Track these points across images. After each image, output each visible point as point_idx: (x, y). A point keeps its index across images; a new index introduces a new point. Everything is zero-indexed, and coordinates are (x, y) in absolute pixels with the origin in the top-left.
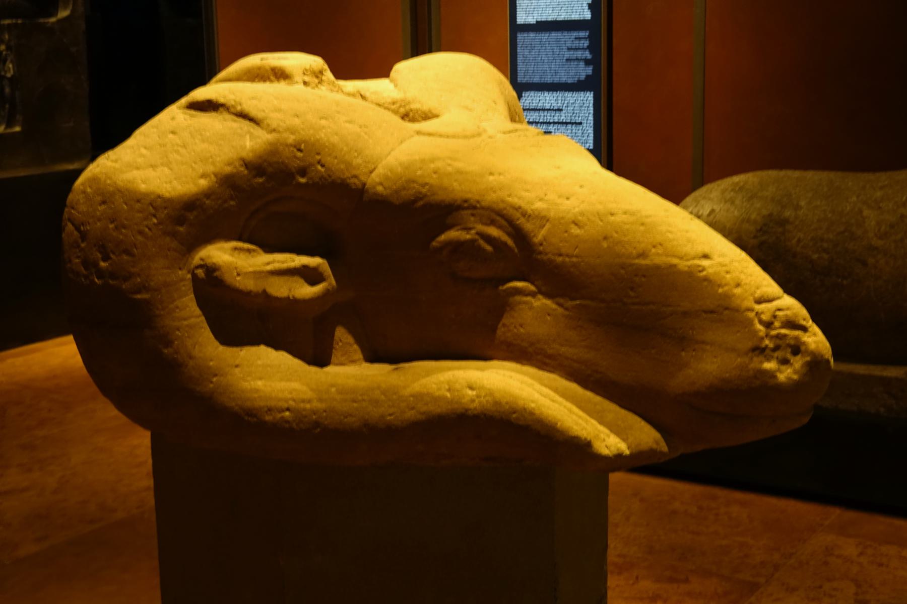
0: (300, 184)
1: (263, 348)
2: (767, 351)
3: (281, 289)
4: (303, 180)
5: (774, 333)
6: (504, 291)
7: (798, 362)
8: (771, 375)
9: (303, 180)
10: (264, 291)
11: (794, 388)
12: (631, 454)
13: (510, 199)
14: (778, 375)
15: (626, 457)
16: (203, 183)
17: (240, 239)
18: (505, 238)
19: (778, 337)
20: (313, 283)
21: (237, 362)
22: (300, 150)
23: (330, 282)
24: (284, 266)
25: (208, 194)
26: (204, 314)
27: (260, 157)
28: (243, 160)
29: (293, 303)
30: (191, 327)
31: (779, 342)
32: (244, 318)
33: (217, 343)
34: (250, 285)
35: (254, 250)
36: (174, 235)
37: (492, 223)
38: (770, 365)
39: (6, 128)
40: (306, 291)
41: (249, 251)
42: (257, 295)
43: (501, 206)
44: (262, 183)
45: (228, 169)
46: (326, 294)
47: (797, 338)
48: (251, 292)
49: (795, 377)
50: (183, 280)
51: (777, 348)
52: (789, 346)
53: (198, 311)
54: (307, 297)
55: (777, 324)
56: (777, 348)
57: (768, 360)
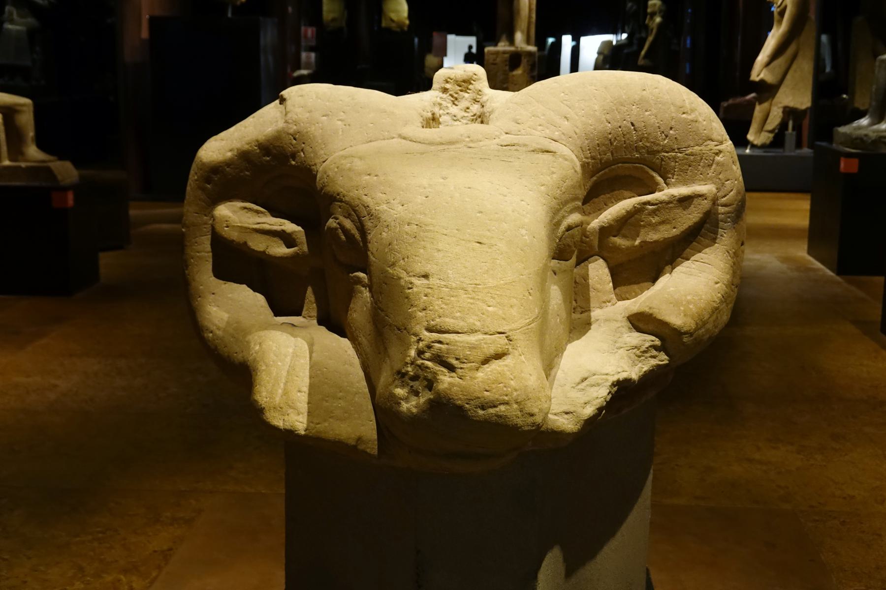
0: (292, 165)
1: (244, 286)
2: (406, 378)
3: (258, 244)
4: (293, 163)
5: (420, 362)
6: (352, 278)
7: (426, 396)
8: (397, 400)
9: (293, 163)
10: (245, 243)
11: (413, 420)
12: (305, 436)
13: (365, 198)
14: (403, 403)
15: (299, 436)
16: (229, 154)
17: (244, 200)
18: (355, 232)
19: (422, 367)
20: (289, 246)
21: (214, 292)
22: (295, 139)
23: (304, 247)
24: (267, 227)
25: (228, 163)
26: (213, 251)
27: (268, 141)
28: (257, 141)
29: (282, 259)
30: (200, 258)
31: (420, 372)
32: (237, 262)
33: (211, 274)
34: (234, 236)
35: (262, 213)
36: (203, 189)
37: (348, 216)
38: (400, 392)
39: (872, 124)
40: (280, 250)
41: (257, 212)
42: (239, 244)
43: (357, 202)
44: (268, 161)
45: (246, 147)
46: (295, 257)
47: (435, 374)
48: (233, 241)
49: (414, 410)
50: (206, 224)
51: (415, 378)
52: (426, 379)
53: (209, 248)
54: (279, 255)
55: (427, 355)
56: (415, 378)
57: (403, 387)
